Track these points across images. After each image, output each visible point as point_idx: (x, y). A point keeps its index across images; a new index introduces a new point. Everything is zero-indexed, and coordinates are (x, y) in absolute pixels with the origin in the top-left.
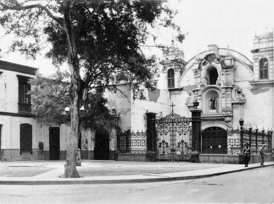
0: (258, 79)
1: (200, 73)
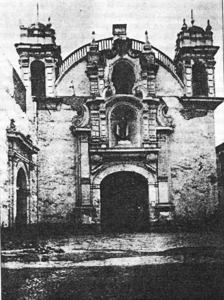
0: (191, 94)
1: (103, 71)
